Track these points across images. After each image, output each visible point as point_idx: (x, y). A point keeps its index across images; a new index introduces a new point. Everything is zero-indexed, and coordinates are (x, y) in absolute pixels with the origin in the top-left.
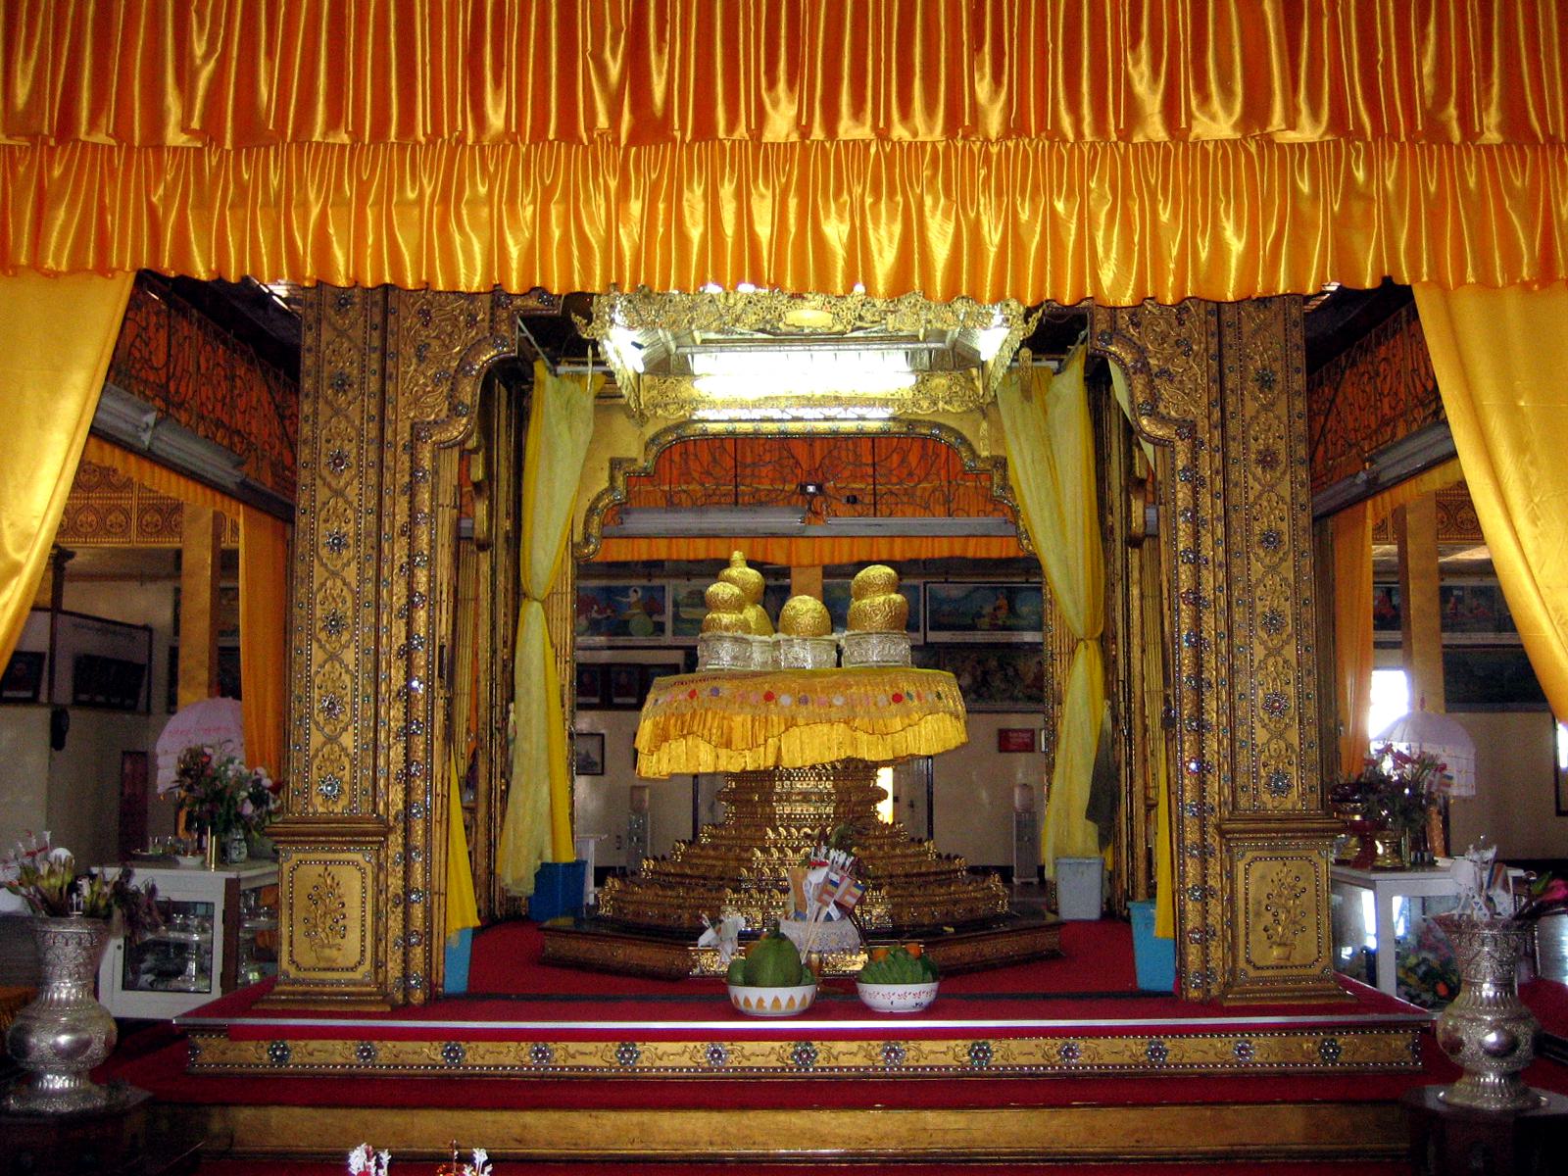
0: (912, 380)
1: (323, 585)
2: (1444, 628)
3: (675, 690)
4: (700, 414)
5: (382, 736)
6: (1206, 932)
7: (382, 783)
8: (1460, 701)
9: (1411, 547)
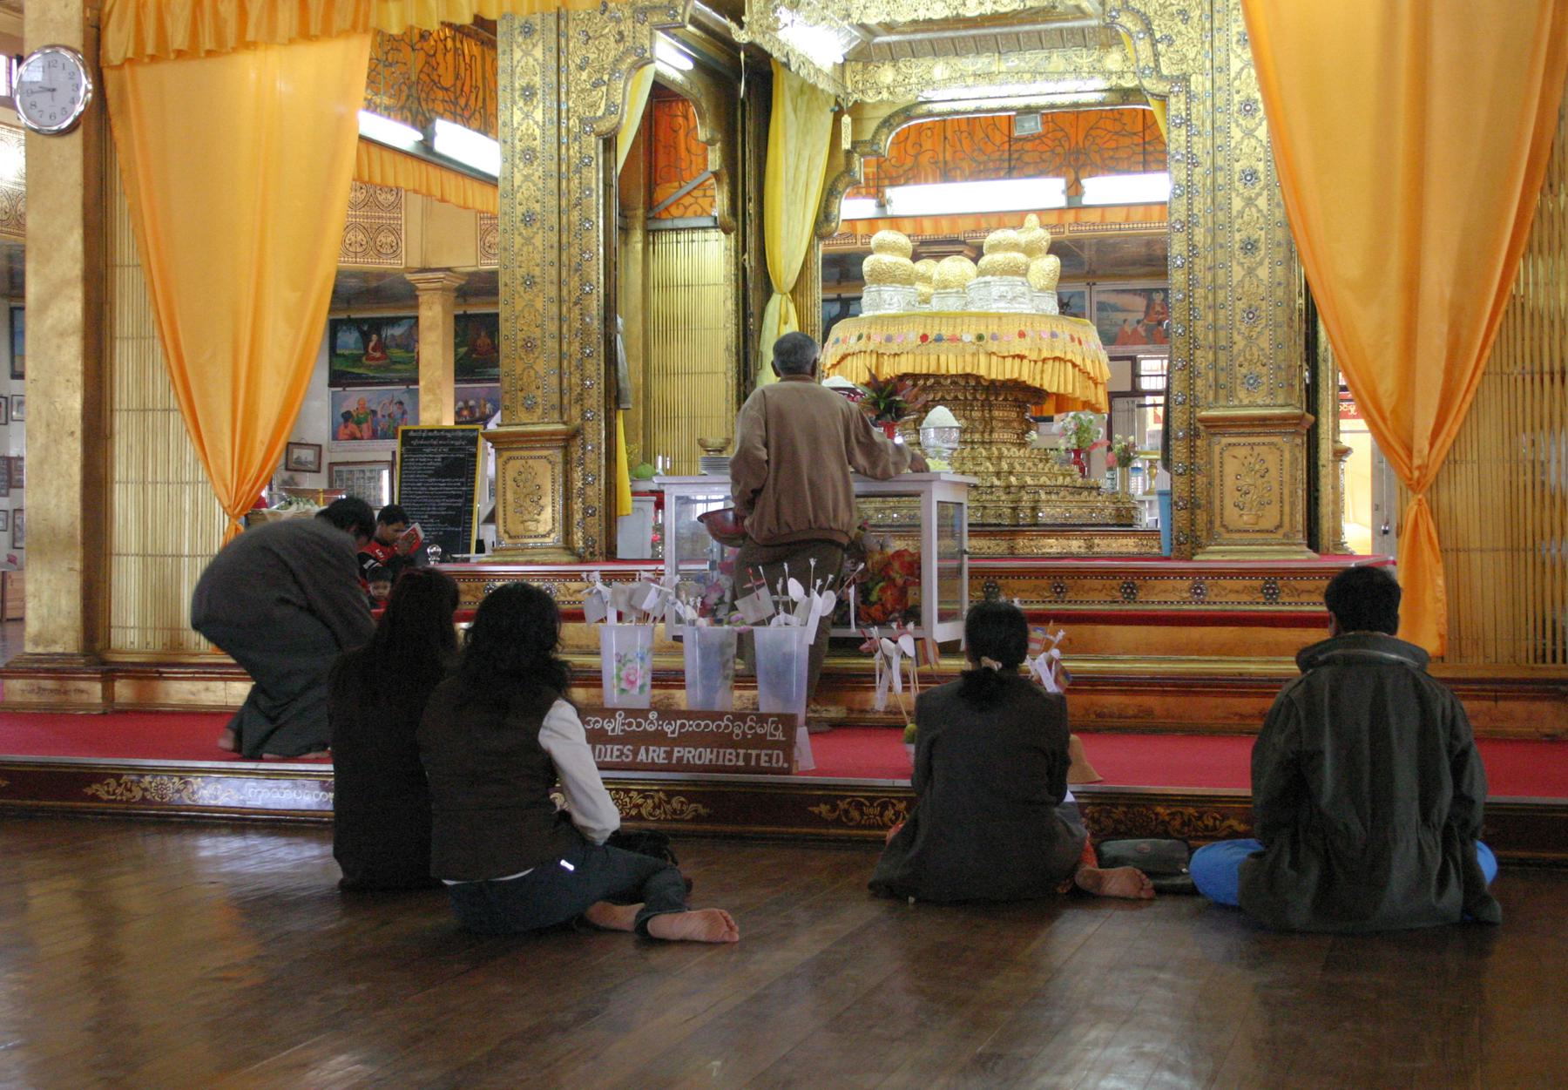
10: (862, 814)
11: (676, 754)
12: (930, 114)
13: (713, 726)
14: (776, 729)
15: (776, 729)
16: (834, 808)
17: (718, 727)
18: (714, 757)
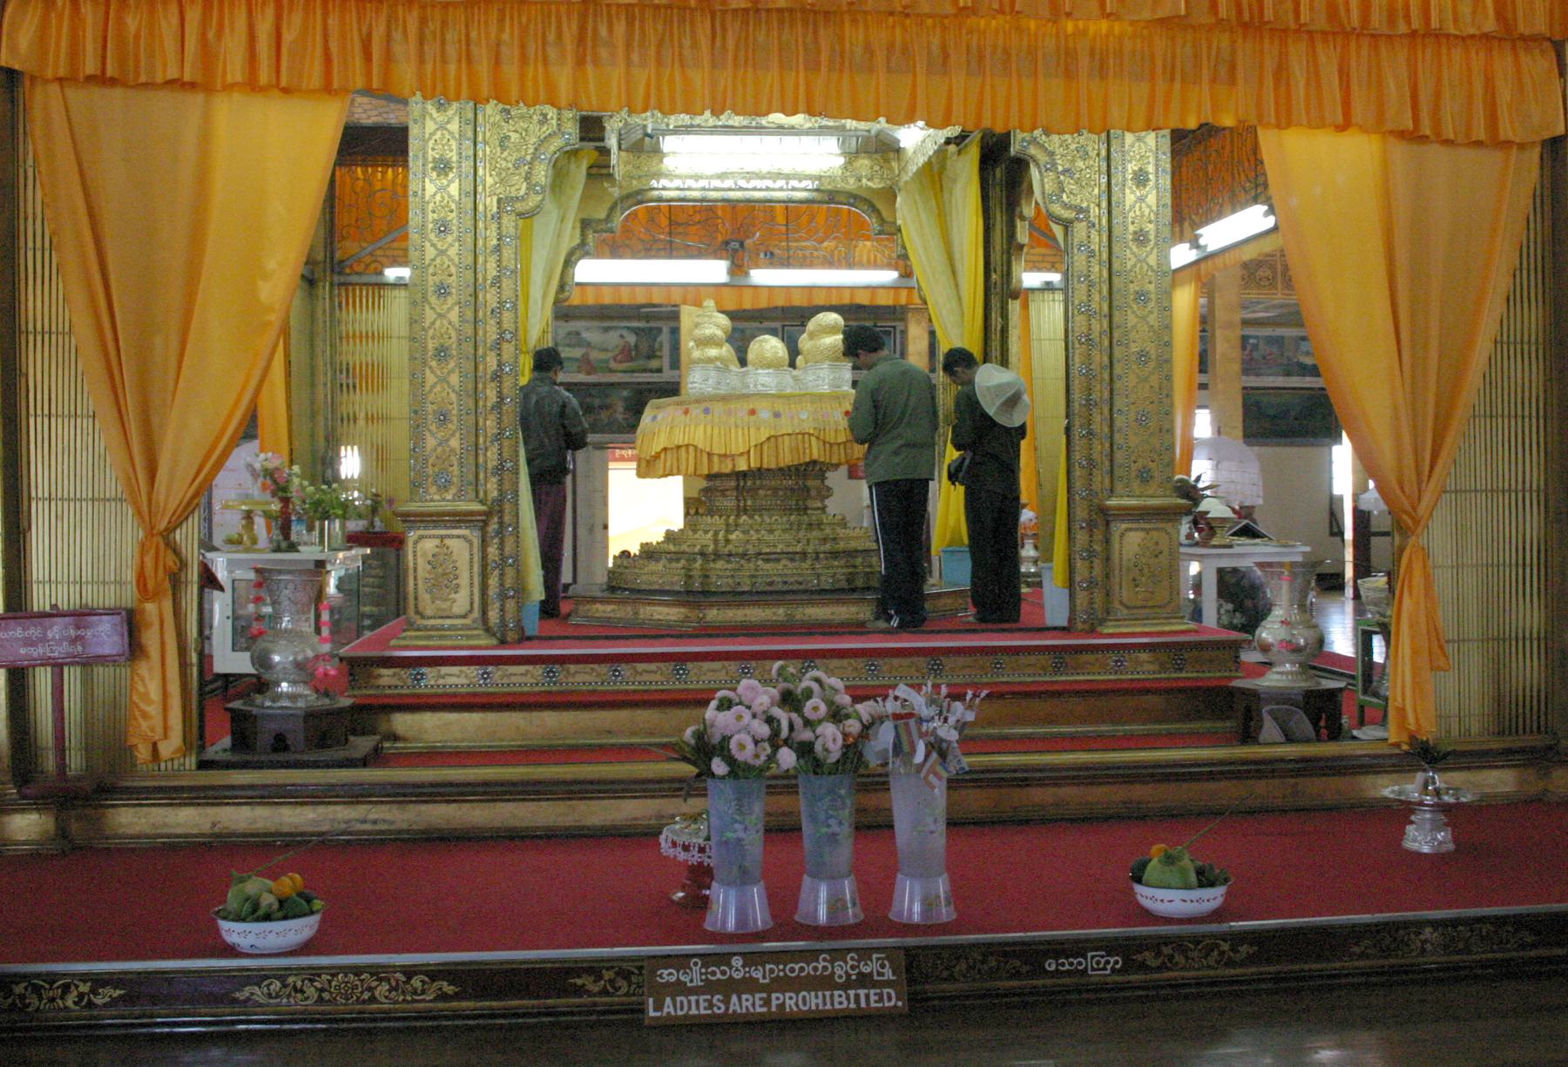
0: (842, 160)
1: (433, 323)
2: (1246, 371)
3: (671, 408)
4: (654, 183)
5: (481, 440)
6: (1092, 583)
7: (482, 476)
8: (1254, 436)
9: (1218, 301)
10: (1187, 958)
11: (774, 1002)
12: (660, 200)
13: (809, 969)
14: (883, 966)
15: (883, 966)
16: (1159, 954)
17: (815, 969)
18: (820, 1001)
